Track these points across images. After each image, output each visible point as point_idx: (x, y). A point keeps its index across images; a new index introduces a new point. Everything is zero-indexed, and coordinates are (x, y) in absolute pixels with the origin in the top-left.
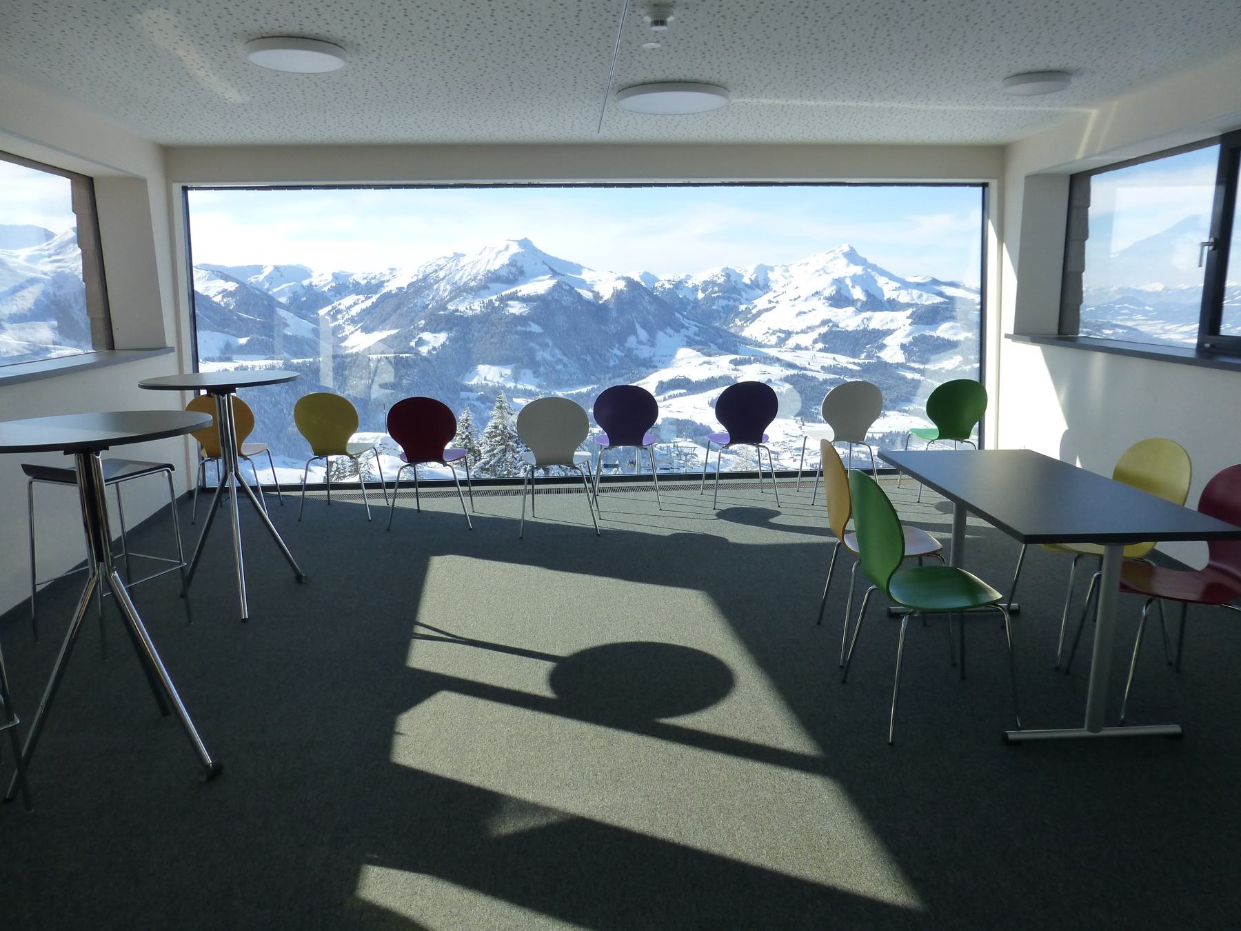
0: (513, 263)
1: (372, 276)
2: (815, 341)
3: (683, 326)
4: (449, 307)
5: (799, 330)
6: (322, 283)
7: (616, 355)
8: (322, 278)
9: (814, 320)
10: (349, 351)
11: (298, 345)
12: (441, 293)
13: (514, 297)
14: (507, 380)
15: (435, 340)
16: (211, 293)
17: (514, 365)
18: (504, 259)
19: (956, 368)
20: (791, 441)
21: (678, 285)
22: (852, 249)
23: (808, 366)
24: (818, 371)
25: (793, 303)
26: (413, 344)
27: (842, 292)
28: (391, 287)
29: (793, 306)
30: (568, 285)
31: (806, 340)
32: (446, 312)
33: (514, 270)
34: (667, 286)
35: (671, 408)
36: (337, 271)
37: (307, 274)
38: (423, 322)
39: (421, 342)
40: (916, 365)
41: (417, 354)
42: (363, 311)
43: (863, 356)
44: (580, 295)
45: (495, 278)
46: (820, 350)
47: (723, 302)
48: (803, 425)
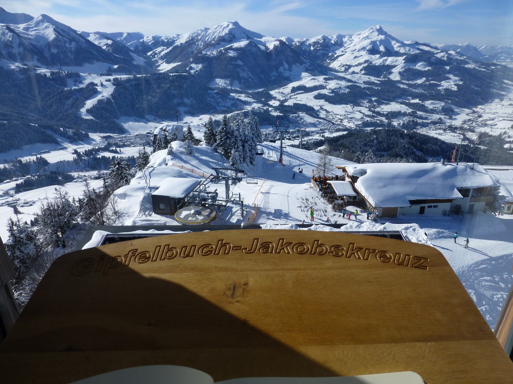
0: (231, 32)
1: (170, 38)
2: (361, 70)
3: (304, 62)
4: (203, 53)
5: (354, 65)
6: (148, 41)
7: (274, 75)
8: (148, 39)
9: (362, 60)
10: (161, 72)
12: (199, 46)
13: (231, 48)
14: (227, 85)
15: (197, 67)
16: (102, 45)
17: (230, 79)
18: (227, 31)
19: (423, 83)
20: (348, 114)
21: (302, 43)
22: (381, 28)
23: (357, 81)
24: (362, 84)
25: (352, 52)
26: (188, 69)
27: (375, 47)
28: (178, 43)
29: (353, 54)
30: (254, 43)
31: (357, 69)
32: (202, 55)
33: (231, 36)
34: (297, 44)
35: (298, 99)
36: (154, 36)
37: (141, 36)
38: (192, 59)
39: (191, 68)
40: (405, 82)
41: (190, 73)
42: (166, 54)
43: (382, 77)
44: (259, 48)
45: (222, 40)
46: (363, 74)
47: (322, 52)
48: (354, 107)
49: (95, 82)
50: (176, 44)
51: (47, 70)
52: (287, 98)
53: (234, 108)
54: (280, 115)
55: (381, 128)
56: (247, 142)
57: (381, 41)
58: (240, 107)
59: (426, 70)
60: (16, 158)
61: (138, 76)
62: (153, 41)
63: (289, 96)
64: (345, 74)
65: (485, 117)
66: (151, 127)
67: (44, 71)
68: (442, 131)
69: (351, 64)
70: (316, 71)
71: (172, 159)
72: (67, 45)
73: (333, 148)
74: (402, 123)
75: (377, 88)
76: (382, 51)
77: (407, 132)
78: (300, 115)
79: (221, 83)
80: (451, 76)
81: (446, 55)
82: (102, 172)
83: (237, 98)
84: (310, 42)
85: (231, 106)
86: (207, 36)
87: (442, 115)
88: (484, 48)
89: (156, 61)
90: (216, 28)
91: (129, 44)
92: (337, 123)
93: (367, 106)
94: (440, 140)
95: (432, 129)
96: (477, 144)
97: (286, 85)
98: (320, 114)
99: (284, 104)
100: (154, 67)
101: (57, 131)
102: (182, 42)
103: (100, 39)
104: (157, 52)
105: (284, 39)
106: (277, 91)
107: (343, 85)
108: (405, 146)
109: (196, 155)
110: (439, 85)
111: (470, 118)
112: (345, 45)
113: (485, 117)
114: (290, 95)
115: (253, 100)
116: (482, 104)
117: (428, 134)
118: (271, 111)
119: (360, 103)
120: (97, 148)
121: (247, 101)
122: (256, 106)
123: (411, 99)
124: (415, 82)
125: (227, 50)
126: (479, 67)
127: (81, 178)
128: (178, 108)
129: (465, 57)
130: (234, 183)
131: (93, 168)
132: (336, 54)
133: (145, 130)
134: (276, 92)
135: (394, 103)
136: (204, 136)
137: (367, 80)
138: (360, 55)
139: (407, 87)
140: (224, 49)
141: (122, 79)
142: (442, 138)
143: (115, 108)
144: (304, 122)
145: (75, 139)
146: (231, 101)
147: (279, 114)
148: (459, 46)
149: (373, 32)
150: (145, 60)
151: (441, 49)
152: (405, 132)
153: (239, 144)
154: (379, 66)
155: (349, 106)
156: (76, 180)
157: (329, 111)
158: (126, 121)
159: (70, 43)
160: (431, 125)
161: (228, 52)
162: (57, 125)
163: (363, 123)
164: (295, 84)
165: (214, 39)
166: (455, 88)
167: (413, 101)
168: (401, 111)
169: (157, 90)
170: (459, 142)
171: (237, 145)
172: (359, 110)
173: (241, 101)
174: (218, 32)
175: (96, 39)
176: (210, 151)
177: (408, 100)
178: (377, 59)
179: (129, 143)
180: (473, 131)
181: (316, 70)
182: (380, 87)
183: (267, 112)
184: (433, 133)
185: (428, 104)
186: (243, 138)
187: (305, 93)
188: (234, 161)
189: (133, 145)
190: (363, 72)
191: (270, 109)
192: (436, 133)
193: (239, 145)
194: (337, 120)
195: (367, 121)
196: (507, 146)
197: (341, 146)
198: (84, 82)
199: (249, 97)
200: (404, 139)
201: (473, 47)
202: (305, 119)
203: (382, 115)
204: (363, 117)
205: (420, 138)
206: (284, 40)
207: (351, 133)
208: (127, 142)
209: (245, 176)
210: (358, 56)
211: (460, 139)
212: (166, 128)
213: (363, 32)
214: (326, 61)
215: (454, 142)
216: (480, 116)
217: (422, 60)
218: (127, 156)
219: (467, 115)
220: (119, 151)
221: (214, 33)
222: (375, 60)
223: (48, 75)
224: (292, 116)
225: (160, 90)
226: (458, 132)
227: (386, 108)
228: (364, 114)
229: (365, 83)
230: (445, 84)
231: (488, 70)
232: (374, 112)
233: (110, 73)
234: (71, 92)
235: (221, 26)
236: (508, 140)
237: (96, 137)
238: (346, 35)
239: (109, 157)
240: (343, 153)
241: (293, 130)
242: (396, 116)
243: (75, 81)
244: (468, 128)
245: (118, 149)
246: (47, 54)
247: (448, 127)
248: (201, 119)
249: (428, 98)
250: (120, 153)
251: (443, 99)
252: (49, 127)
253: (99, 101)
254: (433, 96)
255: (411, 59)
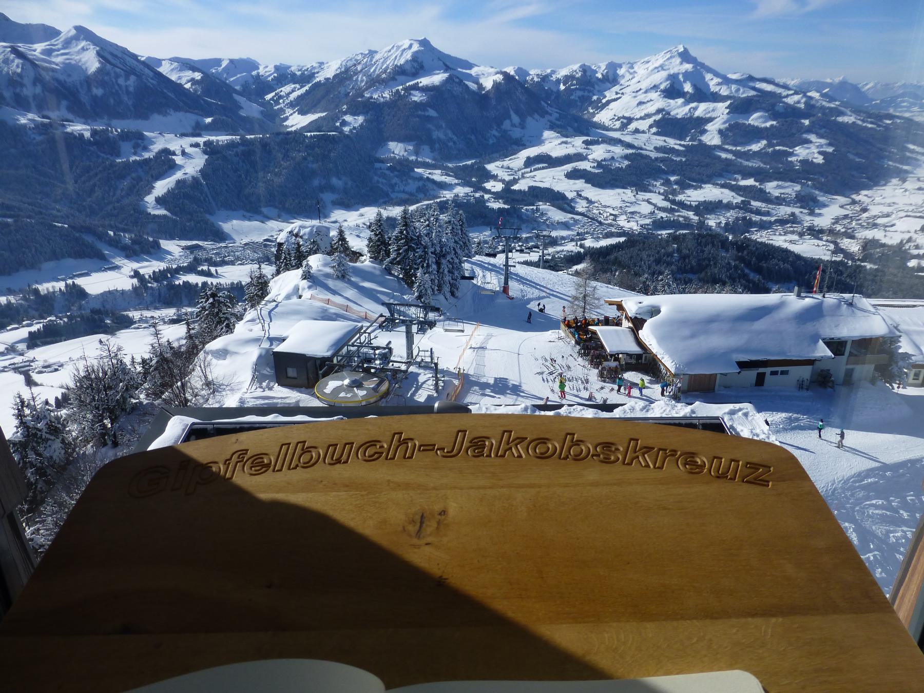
0: (415, 58)
1: (306, 68)
2: (651, 126)
3: (547, 113)
4: (366, 95)
5: (638, 117)
6: (267, 74)
7: (494, 135)
8: (267, 70)
9: (651, 108)
10: (290, 130)
11: (247, 124)
12: (359, 83)
13: (416, 87)
14: (410, 154)
15: (355, 121)
16: (183, 81)
17: (414, 143)
18: (408, 56)
19: (761, 150)
20: (626, 206)
21: (545, 78)
22: (686, 50)
23: (644, 147)
24: (651, 151)
25: (634, 94)
26: (338, 124)
27: (675, 86)
28: (320, 78)
29: (635, 97)
30: (458, 78)
31: (643, 125)
32: (364, 99)
33: (415, 65)
34: (536, 79)
35: (536, 179)
36: (278, 64)
37: (254, 65)
38: (345, 106)
39: (344, 123)
40: (730, 147)
41: (342, 132)
42: (299, 97)
43: (688, 139)
44: (467, 86)
45: (400, 72)
46: (654, 134)
47: (580, 93)
48: (637, 194)
49: (172, 149)
50: (318, 80)
51: (84, 127)
52: (517, 177)
53: (421, 196)
54: (504, 208)
55: (686, 231)
56: (444, 256)
57: (686, 75)
58: (432, 193)
59: (768, 126)
60: (29, 286)
61: (248, 137)
62: (276, 75)
63: (520, 173)
64: (622, 134)
65: (874, 210)
66: (272, 229)
67: (79, 128)
68: (795, 237)
69: (632, 116)
70: (569, 128)
71: (309, 287)
72: (121, 81)
73: (600, 267)
74: (724, 222)
75: (678, 159)
76: (688, 92)
77: (733, 238)
78: (541, 207)
79: (397, 149)
80: (812, 137)
81: (804, 100)
82: (184, 311)
83: (428, 177)
84: (559, 76)
85: (417, 192)
86: (373, 65)
87: (797, 207)
88: (872, 87)
89: (282, 110)
90: (390, 51)
91: (232, 79)
92: (606, 222)
93: (662, 191)
94: (793, 252)
95: (778, 234)
96: (859, 260)
97: (515, 154)
98: (577, 206)
99: (512, 188)
100: (277, 120)
101: (102, 237)
102: (328, 76)
103: (181, 70)
104: (282, 94)
105: (511, 70)
106: (498, 163)
107: (618, 153)
108: (729, 263)
109: (352, 279)
110: (792, 154)
111: (846, 212)
112: (622, 82)
113: (874, 210)
114: (523, 171)
115: (456, 181)
116: (868, 188)
117: (771, 242)
118: (488, 200)
119: (649, 185)
120: (174, 266)
121: (446, 183)
122: (462, 191)
123: (740, 178)
124: (747, 148)
125: (408, 90)
126: (863, 121)
127: (146, 322)
128: (321, 195)
129: (837, 103)
130: (422, 330)
131: (168, 304)
132: (605, 97)
133: (261, 234)
134: (498, 167)
135: (710, 186)
136: (368, 246)
137: (661, 144)
138: (648, 99)
139: (734, 158)
140: (403, 89)
141: (221, 143)
142: (796, 249)
143: (207, 196)
144: (547, 220)
145: (134, 252)
146: (416, 182)
147: (502, 206)
148: (827, 83)
149: (671, 57)
150: (262, 108)
151: (794, 88)
152: (730, 238)
153: (430, 259)
154: (683, 119)
155: (628, 191)
156: (136, 325)
157: (593, 200)
158: (227, 219)
159: (127, 78)
160: (777, 226)
161: (410, 94)
162: (103, 226)
163: (654, 222)
164: (532, 152)
165: (385, 71)
166: (820, 160)
167: (743, 183)
168: (722, 201)
169: (282, 163)
170: (827, 257)
171: (427, 262)
172: (646, 198)
173: (434, 182)
174: (393, 57)
175: (172, 70)
176: (378, 272)
177: (735, 180)
178: (679, 107)
179: (232, 258)
180: (852, 237)
181: (569, 126)
182: (685, 156)
183: (481, 202)
184: (780, 240)
185: (771, 187)
186: (438, 249)
187: (550, 168)
188: (421, 291)
189: (240, 262)
190: (654, 130)
191: (486, 196)
192: (786, 241)
193: (430, 262)
194: (607, 217)
195: (662, 218)
196: (912, 263)
197: (614, 264)
198: (151, 147)
199: (449, 176)
200: (727, 251)
201: (852, 85)
202: (550, 214)
203: (688, 208)
204: (654, 212)
205: (757, 249)
206: (512, 73)
207: (633, 241)
208: (229, 256)
209: (442, 317)
210: (645, 101)
211: (828, 250)
212: (299, 230)
213: (653, 59)
214: (587, 109)
215: (817, 257)
216: (865, 210)
217: (761, 108)
218: (229, 282)
219: (842, 207)
220: (214, 273)
221: (386, 59)
222: (675, 109)
223: (87, 135)
224: (527, 210)
225: (288, 163)
226: (825, 238)
227: (695, 196)
228: (655, 205)
229: (657, 149)
230: (801, 152)
231: (879, 126)
232: (673, 202)
233: (198, 132)
234: (128, 166)
235: (398, 47)
236: (915, 252)
237: (174, 247)
238: (624, 63)
239: (197, 284)
240: (618, 275)
241: (528, 235)
242: (713, 208)
243: (136, 146)
244: (843, 230)
245: (213, 269)
246: (84, 98)
247: (807, 230)
248: (362, 215)
249: (771, 177)
250: (217, 276)
251: (799, 178)
252: (89, 230)
253: (178, 182)
254: (780, 173)
255: (741, 107)
